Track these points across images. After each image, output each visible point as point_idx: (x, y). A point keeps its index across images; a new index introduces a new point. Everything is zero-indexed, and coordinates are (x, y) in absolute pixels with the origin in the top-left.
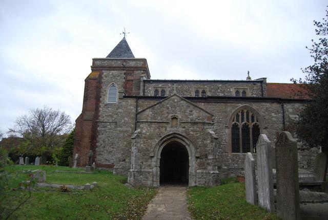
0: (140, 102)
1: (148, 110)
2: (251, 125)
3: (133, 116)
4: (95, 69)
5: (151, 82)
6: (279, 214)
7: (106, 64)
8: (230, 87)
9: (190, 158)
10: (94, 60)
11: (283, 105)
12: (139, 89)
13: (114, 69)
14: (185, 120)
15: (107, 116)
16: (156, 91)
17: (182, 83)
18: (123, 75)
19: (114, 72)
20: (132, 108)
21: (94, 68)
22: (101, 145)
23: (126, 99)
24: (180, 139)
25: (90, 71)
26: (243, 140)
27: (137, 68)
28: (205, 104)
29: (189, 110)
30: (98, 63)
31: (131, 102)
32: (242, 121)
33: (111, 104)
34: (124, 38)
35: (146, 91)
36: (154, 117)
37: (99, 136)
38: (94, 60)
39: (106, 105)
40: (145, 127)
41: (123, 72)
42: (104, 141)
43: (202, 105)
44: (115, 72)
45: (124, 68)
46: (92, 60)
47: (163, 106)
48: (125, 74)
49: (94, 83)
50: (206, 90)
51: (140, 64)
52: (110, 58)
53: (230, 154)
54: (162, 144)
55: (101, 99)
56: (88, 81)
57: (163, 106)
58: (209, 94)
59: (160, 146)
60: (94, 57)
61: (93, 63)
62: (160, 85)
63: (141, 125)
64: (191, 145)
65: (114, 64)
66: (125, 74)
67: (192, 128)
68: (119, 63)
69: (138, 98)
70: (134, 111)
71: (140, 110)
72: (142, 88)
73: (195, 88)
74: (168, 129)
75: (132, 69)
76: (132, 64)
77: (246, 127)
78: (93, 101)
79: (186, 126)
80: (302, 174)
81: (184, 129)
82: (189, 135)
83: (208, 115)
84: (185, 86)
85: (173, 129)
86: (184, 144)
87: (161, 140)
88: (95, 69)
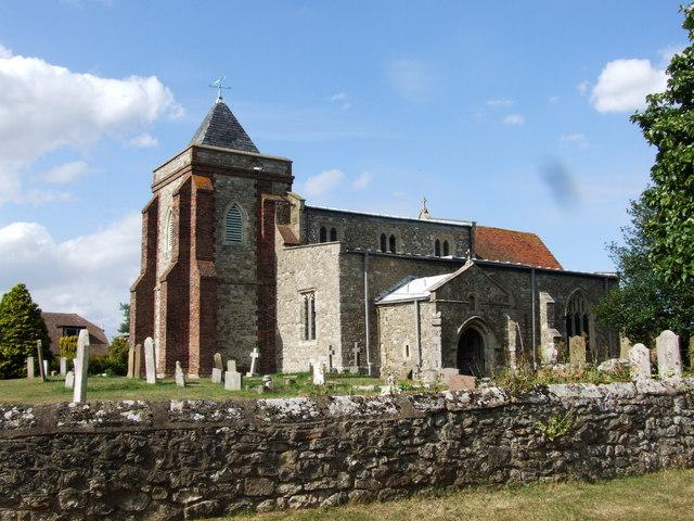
39: (225, 248)
41: (253, 182)
42: (227, 322)
44: (237, 181)
48: (255, 186)
51: (281, 171)
62: (330, 219)
66: (255, 186)
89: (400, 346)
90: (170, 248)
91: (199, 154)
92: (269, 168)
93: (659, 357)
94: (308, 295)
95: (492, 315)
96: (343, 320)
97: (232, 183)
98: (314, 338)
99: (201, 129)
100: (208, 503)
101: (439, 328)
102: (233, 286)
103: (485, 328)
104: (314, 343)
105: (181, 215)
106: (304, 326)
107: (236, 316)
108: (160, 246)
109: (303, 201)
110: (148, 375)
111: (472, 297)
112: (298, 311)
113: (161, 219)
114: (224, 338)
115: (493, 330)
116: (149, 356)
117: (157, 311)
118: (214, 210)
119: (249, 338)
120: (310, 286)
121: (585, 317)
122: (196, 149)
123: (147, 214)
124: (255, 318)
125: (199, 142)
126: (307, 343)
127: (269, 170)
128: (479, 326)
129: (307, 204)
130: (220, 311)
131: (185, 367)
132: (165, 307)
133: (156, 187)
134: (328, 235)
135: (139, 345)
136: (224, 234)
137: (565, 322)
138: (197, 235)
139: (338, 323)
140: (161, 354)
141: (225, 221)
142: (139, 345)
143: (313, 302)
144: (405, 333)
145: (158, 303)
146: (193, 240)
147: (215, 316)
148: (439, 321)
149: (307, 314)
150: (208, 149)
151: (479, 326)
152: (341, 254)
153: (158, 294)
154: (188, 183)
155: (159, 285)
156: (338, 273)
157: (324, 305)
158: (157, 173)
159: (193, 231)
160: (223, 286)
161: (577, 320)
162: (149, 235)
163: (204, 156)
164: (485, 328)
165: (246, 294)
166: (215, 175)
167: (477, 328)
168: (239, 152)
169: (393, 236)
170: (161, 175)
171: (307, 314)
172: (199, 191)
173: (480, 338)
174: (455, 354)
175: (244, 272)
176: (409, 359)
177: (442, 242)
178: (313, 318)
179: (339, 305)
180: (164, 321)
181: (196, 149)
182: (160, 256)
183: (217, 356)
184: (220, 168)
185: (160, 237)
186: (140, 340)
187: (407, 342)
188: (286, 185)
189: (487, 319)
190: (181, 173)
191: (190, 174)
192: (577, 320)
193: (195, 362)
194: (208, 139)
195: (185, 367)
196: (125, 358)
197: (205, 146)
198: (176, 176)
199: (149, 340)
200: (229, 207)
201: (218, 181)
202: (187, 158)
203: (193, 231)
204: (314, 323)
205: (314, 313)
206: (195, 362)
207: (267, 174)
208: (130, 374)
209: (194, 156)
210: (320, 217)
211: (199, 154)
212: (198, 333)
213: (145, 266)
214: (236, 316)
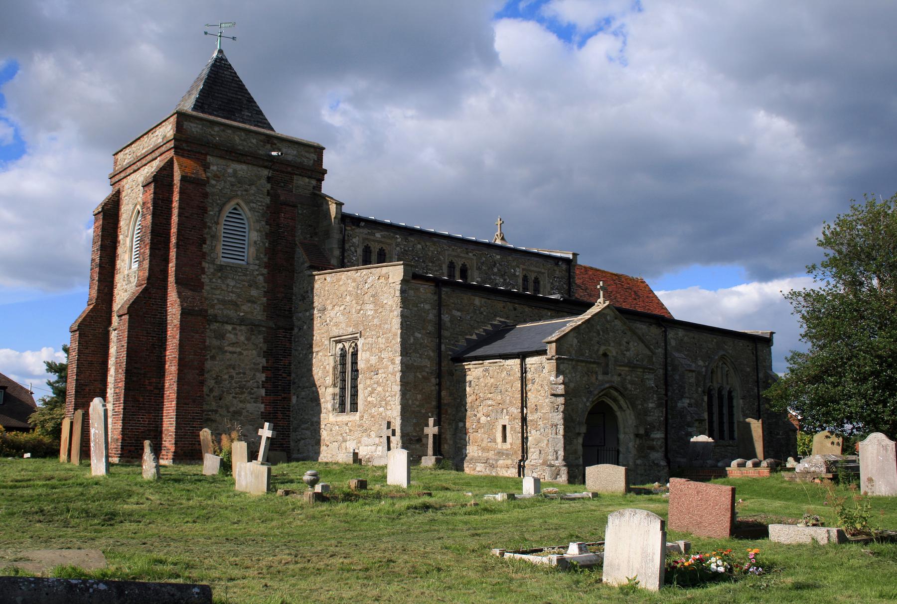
0: (451, 297)
5: (362, 224)
8: (514, 264)
11: (665, 332)
15: (223, 302)
18: (263, 181)
20: (427, 307)
22: (211, 390)
29: (625, 340)
33: (234, 269)
35: (347, 246)
39: (221, 268)
40: (567, 371)
41: (266, 173)
42: (218, 380)
44: (242, 169)
48: (269, 179)
51: (309, 159)
62: (378, 235)
64: (628, 412)
66: (269, 179)
73: (449, 255)
75: (289, 169)
80: (658, 439)
83: (649, 353)
84: (432, 249)
85: (607, 378)
89: (491, 425)
90: (135, 266)
91: (186, 125)
92: (291, 154)
93: (813, 450)
94: (347, 345)
95: (632, 383)
96: (404, 383)
97: (235, 171)
98: (354, 408)
99: (192, 88)
100: (276, 142)
101: (561, 400)
102: (229, 328)
103: (622, 402)
104: (356, 417)
105: (154, 215)
106: (337, 390)
107: (233, 372)
108: (119, 264)
109: (339, 205)
110: (94, 461)
111: (605, 355)
112: (330, 369)
113: (122, 223)
114: (214, 405)
115: (633, 406)
116: (96, 431)
117: (112, 361)
118: (204, 210)
119: (251, 407)
120: (350, 330)
121: (730, 392)
122: (181, 116)
123: (101, 216)
124: (262, 377)
125: (188, 106)
126: (344, 418)
127: (290, 158)
128: (615, 400)
129: (346, 210)
130: (209, 364)
131: (157, 450)
132: (124, 354)
133: (117, 178)
134: (374, 257)
135: (80, 412)
136: (220, 248)
137: (706, 398)
138: (178, 245)
139: (397, 388)
140: (115, 427)
141: (221, 228)
142: (80, 412)
143: (355, 354)
144: (500, 407)
145: (113, 350)
146: (173, 254)
147: (202, 371)
148: (561, 389)
149: (343, 372)
150: (201, 119)
151: (615, 400)
152: (404, 282)
153: (113, 335)
154: (167, 168)
155: (115, 320)
156: (398, 311)
157: (374, 360)
158: (120, 156)
159: (173, 240)
160: (215, 326)
161: (720, 397)
162: (103, 248)
163: (194, 128)
164: (622, 402)
165: (248, 339)
166: (210, 159)
167: (615, 407)
168: (247, 126)
169: (464, 265)
170: (126, 158)
171: (343, 372)
172: (184, 179)
173: (615, 418)
174: (580, 440)
175: (246, 307)
176: (507, 446)
177: (532, 277)
178: (355, 379)
179: (398, 360)
180: (122, 376)
181: (181, 116)
182: (119, 279)
183: (206, 434)
184: (216, 147)
185: (120, 250)
186: (83, 404)
187: (505, 420)
188: (314, 182)
189: (626, 389)
190: (157, 153)
191: (171, 153)
192: (720, 397)
193: (169, 442)
194: (198, 106)
195: (157, 450)
196: (57, 432)
197: (194, 113)
198: (149, 158)
199: (97, 402)
200: (229, 208)
201: (214, 168)
202: (168, 130)
203: (173, 240)
204: (355, 387)
205: (355, 371)
206: (169, 442)
207: (288, 164)
208: (63, 456)
209: (179, 127)
210: (363, 232)
211: (186, 125)
212: (174, 396)
213: (94, 293)
214: (233, 372)
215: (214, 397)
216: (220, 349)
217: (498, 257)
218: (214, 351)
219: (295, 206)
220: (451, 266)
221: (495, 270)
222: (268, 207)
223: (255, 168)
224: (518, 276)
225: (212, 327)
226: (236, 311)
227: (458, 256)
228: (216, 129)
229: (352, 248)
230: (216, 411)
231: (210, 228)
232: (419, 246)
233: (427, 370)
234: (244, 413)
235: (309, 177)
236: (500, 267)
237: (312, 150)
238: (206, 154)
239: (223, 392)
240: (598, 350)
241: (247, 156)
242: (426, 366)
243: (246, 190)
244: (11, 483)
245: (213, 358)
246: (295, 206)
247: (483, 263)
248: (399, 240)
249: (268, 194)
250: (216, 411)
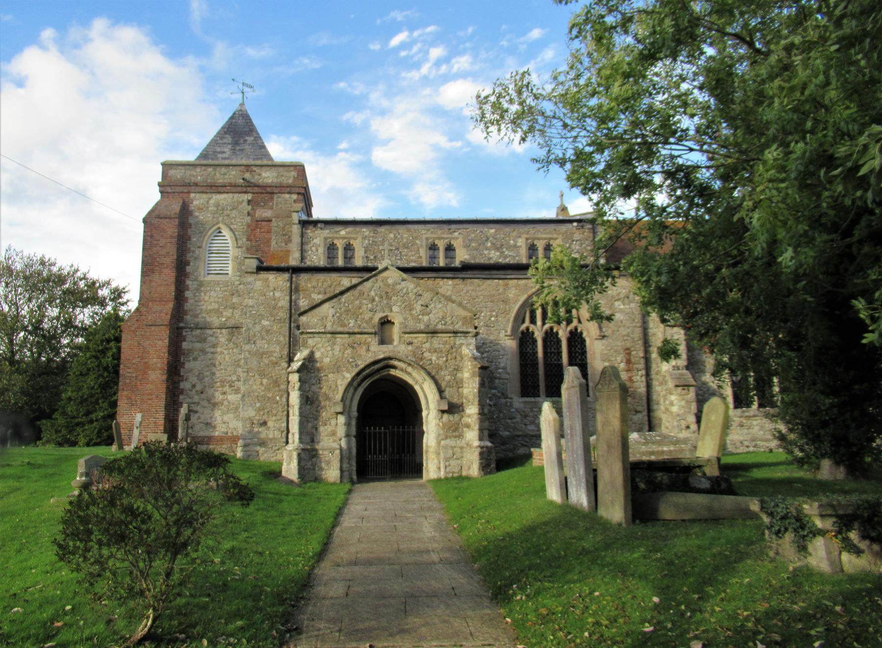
1: (326, 306)
2: (563, 333)
3: (283, 314)
4: (169, 190)
6: (642, 196)
7: (198, 175)
9: (424, 414)
10: (167, 166)
12: (289, 241)
13: (222, 189)
14: (412, 325)
16: (331, 248)
17: (398, 227)
18: (245, 204)
19: (216, 198)
21: (165, 187)
23: (263, 275)
24: (402, 370)
25: (158, 197)
26: (546, 364)
27: (282, 188)
28: (456, 281)
30: (177, 174)
31: (280, 281)
32: (544, 324)
34: (242, 104)
36: (340, 321)
37: (187, 365)
38: (167, 166)
40: (320, 345)
43: (447, 286)
45: (248, 186)
46: (161, 167)
47: (362, 294)
49: (171, 229)
50: (455, 243)
51: (289, 178)
52: (205, 162)
53: (518, 402)
54: (359, 385)
55: (189, 269)
56: (152, 222)
57: (362, 294)
58: (462, 256)
59: (356, 389)
60: (163, 160)
61: (165, 175)
62: (343, 233)
63: (311, 342)
65: (221, 177)
67: (427, 345)
68: (233, 176)
69: (296, 270)
70: (284, 303)
71: (303, 304)
72: (296, 239)
74: (372, 348)
76: (268, 177)
77: (551, 338)
78: (168, 275)
79: (415, 341)
81: (410, 348)
82: (421, 359)
86: (410, 381)
87: (358, 374)
88: (169, 190)
91: (172, 172)
165: (230, 340)
215: (197, 391)
216: (203, 351)
217: (493, 231)
218: (196, 353)
219: (270, 221)
220: (433, 247)
221: (489, 244)
222: (249, 226)
223: (236, 195)
224: (520, 247)
225: (194, 333)
226: (218, 317)
227: (440, 238)
228: (198, 170)
229: (314, 249)
230: (198, 404)
231: (194, 252)
232: (392, 236)
233: (275, 355)
234: (226, 403)
235: (289, 193)
236: (495, 241)
237: (292, 168)
238: (189, 192)
239: (205, 387)
240: (371, 319)
241: (225, 186)
242: (274, 352)
243: (228, 216)
244: (472, 436)
245: (195, 359)
246: (270, 221)
247: (471, 240)
248: (367, 234)
249: (249, 214)
250: (198, 404)
